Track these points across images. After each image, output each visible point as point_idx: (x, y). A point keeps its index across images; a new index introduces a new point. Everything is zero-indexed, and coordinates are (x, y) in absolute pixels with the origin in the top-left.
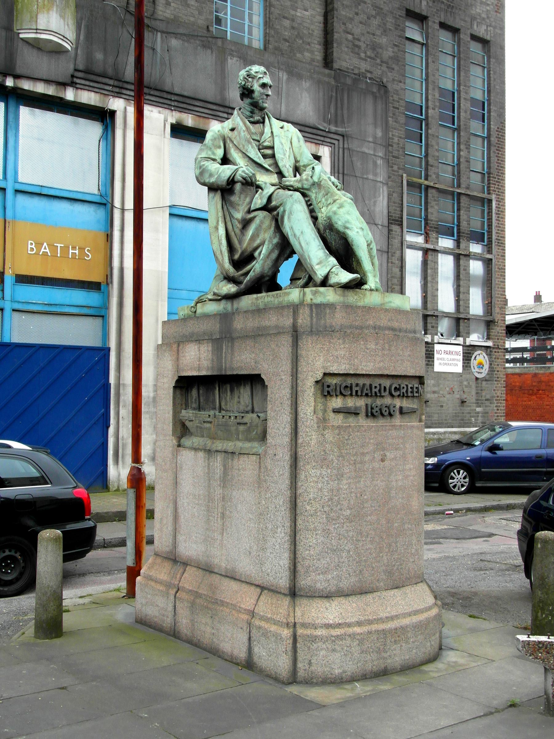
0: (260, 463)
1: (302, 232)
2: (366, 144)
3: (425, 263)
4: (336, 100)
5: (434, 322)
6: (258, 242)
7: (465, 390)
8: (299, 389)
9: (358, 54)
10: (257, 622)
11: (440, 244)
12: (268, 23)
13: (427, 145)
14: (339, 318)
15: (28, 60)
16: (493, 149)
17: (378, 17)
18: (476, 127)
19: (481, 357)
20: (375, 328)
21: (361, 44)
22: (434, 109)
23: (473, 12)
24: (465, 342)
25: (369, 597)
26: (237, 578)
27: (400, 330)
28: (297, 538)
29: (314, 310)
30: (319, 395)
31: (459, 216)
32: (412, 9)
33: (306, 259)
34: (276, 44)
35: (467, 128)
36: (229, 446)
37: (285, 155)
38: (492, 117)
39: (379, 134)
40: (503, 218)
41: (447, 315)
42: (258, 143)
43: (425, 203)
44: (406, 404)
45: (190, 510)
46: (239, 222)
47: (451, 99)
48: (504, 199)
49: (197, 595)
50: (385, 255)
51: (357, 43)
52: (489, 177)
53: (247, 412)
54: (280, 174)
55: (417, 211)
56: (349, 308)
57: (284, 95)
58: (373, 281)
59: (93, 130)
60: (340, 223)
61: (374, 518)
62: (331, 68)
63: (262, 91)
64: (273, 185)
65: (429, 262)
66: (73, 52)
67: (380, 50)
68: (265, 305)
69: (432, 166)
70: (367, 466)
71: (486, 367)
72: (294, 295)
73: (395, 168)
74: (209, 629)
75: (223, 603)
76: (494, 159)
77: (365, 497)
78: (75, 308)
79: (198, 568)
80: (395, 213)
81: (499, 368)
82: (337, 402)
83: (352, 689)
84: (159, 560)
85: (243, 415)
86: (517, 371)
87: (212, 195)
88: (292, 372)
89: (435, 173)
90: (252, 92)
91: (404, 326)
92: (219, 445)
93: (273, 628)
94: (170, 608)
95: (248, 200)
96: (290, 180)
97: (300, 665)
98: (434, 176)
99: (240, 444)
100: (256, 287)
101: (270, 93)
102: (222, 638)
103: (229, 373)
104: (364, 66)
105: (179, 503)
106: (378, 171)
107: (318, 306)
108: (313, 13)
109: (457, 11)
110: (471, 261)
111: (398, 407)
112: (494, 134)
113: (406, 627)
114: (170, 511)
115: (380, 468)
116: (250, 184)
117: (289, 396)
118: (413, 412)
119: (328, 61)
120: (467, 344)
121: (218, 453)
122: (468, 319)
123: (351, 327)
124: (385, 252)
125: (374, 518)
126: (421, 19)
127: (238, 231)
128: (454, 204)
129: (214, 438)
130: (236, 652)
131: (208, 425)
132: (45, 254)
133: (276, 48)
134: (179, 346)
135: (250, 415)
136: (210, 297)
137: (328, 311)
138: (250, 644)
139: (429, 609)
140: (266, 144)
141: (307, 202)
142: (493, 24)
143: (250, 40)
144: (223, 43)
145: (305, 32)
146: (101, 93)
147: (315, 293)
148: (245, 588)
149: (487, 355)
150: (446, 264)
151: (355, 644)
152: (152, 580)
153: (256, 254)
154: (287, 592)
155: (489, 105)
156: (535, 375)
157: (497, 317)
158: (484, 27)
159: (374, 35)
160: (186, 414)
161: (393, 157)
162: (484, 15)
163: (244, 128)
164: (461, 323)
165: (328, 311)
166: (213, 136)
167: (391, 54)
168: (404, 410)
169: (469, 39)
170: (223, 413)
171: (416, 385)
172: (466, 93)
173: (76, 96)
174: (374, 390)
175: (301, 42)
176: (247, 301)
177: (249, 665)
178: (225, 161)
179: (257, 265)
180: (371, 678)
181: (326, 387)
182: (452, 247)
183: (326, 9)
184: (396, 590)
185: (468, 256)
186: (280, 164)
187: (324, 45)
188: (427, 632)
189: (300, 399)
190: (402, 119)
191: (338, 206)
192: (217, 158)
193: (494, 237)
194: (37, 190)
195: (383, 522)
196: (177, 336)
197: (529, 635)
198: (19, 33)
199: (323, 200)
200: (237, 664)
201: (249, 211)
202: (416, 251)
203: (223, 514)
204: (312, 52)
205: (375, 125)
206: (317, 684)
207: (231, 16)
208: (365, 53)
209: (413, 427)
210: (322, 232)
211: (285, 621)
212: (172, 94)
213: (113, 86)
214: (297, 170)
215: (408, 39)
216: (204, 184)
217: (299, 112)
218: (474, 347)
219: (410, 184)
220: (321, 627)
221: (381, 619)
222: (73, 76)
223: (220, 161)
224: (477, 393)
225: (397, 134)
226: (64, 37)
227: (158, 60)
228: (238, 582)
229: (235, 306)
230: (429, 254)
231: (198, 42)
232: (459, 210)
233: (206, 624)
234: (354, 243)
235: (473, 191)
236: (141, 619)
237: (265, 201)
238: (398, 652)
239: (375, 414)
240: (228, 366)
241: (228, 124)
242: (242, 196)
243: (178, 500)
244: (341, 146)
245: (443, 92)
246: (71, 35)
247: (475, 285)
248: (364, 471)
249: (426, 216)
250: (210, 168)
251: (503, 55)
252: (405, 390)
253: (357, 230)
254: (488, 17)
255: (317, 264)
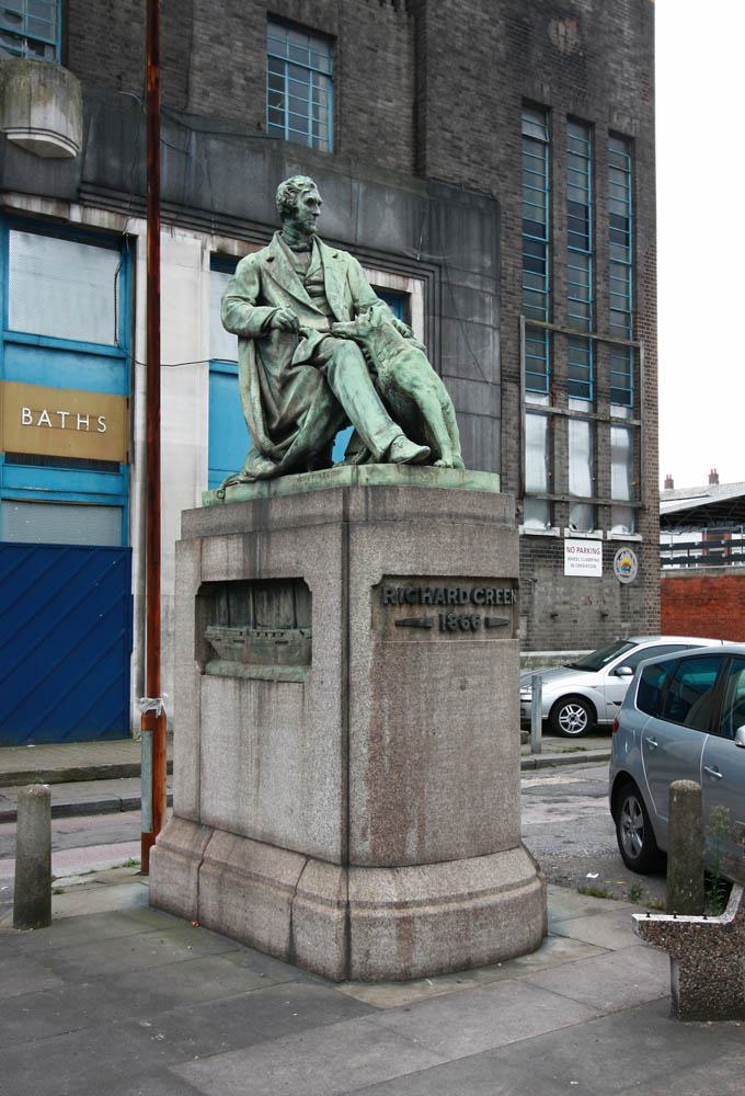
0: (303, 692)
1: (357, 393)
2: (471, 276)
3: (551, 433)
4: (430, 218)
5: (564, 510)
6: (301, 405)
7: (607, 599)
8: (352, 596)
9: (459, 158)
10: (300, 901)
11: (570, 408)
12: (339, 119)
13: (552, 277)
14: (402, 504)
15: (21, 169)
16: (640, 280)
17: (485, 109)
18: (617, 252)
19: (626, 557)
20: (450, 516)
21: (462, 144)
22: (560, 229)
23: (612, 100)
24: (605, 536)
25: (447, 867)
26: (277, 844)
27: (485, 519)
28: (351, 791)
29: (370, 493)
30: (378, 604)
31: (595, 370)
32: (530, 96)
33: (362, 427)
34: (350, 146)
35: (605, 253)
36: (265, 671)
37: (338, 292)
38: (638, 239)
39: (488, 262)
40: (655, 372)
41: (581, 501)
42: (302, 277)
43: (550, 353)
44: (494, 614)
45: (219, 757)
46: (278, 381)
47: (581, 218)
48: (655, 347)
49: (226, 868)
50: (497, 423)
51: (457, 143)
52: (635, 318)
53: (289, 628)
54: (332, 317)
55: (540, 365)
56: (414, 489)
57: (360, 213)
58: (448, 457)
59: (109, 262)
60: (406, 380)
61: (452, 763)
62: (423, 177)
63: (308, 209)
64: (321, 332)
65: (556, 431)
66: (79, 158)
67: (488, 152)
68: (310, 488)
69: (559, 304)
70: (441, 695)
71: (635, 568)
72: (344, 474)
73: (510, 307)
74: (240, 913)
75: (257, 878)
76: (641, 294)
77: (440, 736)
78: (85, 496)
79: (228, 832)
80: (509, 367)
81: (652, 570)
82: (402, 613)
83: (423, 988)
84: (179, 824)
85: (282, 631)
86: (682, 574)
87: (243, 345)
88: (342, 574)
89: (562, 314)
90: (296, 210)
91: (490, 513)
92: (254, 671)
93: (320, 909)
94: (193, 886)
95: (288, 351)
96: (345, 324)
97: (355, 957)
98: (561, 318)
99: (278, 669)
100: (300, 464)
101: (319, 212)
102: (257, 924)
103: (264, 576)
104: (467, 174)
105: (204, 748)
106: (487, 311)
107: (374, 488)
108: (399, 103)
109: (590, 99)
110: (613, 430)
111: (482, 617)
112: (641, 262)
113: (496, 906)
114: (192, 759)
115: (459, 698)
116: (292, 332)
117: (338, 605)
118: (504, 624)
119: (419, 167)
120: (609, 538)
121: (253, 682)
122: (610, 506)
123: (418, 514)
124: (497, 418)
125: (452, 763)
126: (542, 110)
127: (276, 392)
128: (588, 354)
129: (247, 662)
130: (274, 942)
131: (239, 645)
132: (45, 425)
133: (351, 152)
134: (202, 541)
135: (292, 631)
136: (242, 478)
137: (388, 494)
138: (291, 930)
139: (528, 882)
140: (314, 278)
141: (364, 354)
142: (640, 115)
143: (315, 141)
144: (279, 145)
145: (388, 129)
146: (118, 213)
147: (371, 471)
148: (286, 857)
149: (635, 553)
150: (579, 433)
151: (427, 929)
152: (168, 849)
153: (299, 422)
154: (338, 861)
155: (634, 222)
156: (706, 579)
157: (648, 503)
158: (627, 120)
159: (479, 132)
160: (213, 631)
161: (507, 292)
162: (627, 105)
163: (285, 258)
164: (601, 512)
165: (388, 494)
166: (245, 268)
167: (502, 157)
168: (492, 623)
169: (607, 136)
170: (259, 629)
171: (507, 590)
172: (604, 207)
173: (83, 216)
174: (450, 596)
175: (383, 142)
176: (288, 483)
177: (291, 958)
178: (261, 300)
179: (300, 436)
180: (449, 973)
181: (389, 593)
182: (586, 411)
183: (416, 99)
184: (483, 858)
185: (609, 422)
186: (332, 305)
187: (49, 201)
188: (524, 913)
189: (353, 609)
190: (518, 244)
191: (403, 357)
192: (249, 297)
193: (643, 397)
194: (33, 341)
195: (465, 767)
196: (199, 534)
197: (648, 914)
198: (7, 134)
199: (385, 350)
200: (276, 958)
201: (290, 366)
202: (539, 417)
203: (258, 760)
204: (397, 156)
205: (482, 251)
206: (377, 982)
207: (290, 109)
208: (468, 156)
209: (503, 643)
210: (383, 392)
211: (335, 899)
212: (212, 213)
213: (131, 203)
214: (355, 311)
215: (525, 137)
216: (232, 331)
217: (380, 235)
218: (617, 543)
219: (530, 329)
220: (382, 907)
221: (462, 895)
222: (79, 191)
223: (253, 300)
224: (622, 604)
225: (512, 263)
226: (66, 138)
227: (193, 170)
228: (278, 850)
229: (273, 489)
230: (556, 422)
231: (246, 144)
232: (595, 362)
233: (237, 906)
234: (425, 406)
235: (613, 336)
236: (156, 902)
237: (310, 352)
238: (485, 939)
239: (452, 627)
240: (263, 567)
241: (265, 252)
242: (282, 346)
243: (203, 744)
244: (437, 279)
245: (573, 206)
246: (75, 134)
247: (618, 462)
248: (437, 702)
249: (552, 371)
250: (239, 310)
251: (653, 157)
252: (491, 597)
253: (428, 389)
254: (632, 107)
255: (377, 434)
